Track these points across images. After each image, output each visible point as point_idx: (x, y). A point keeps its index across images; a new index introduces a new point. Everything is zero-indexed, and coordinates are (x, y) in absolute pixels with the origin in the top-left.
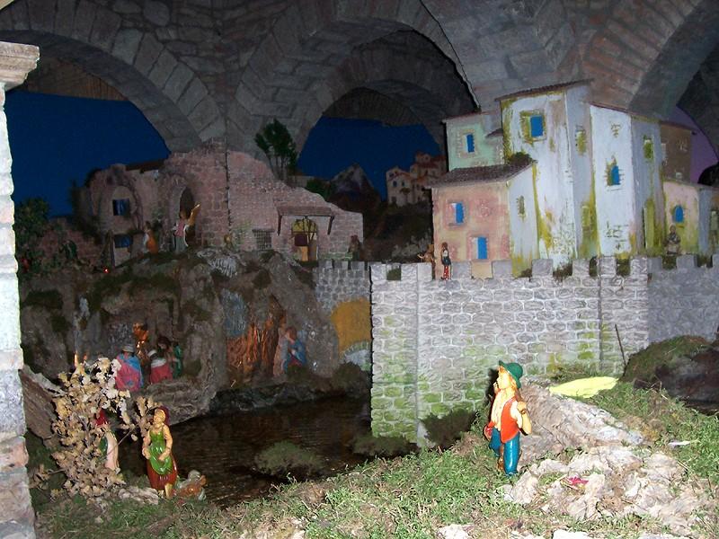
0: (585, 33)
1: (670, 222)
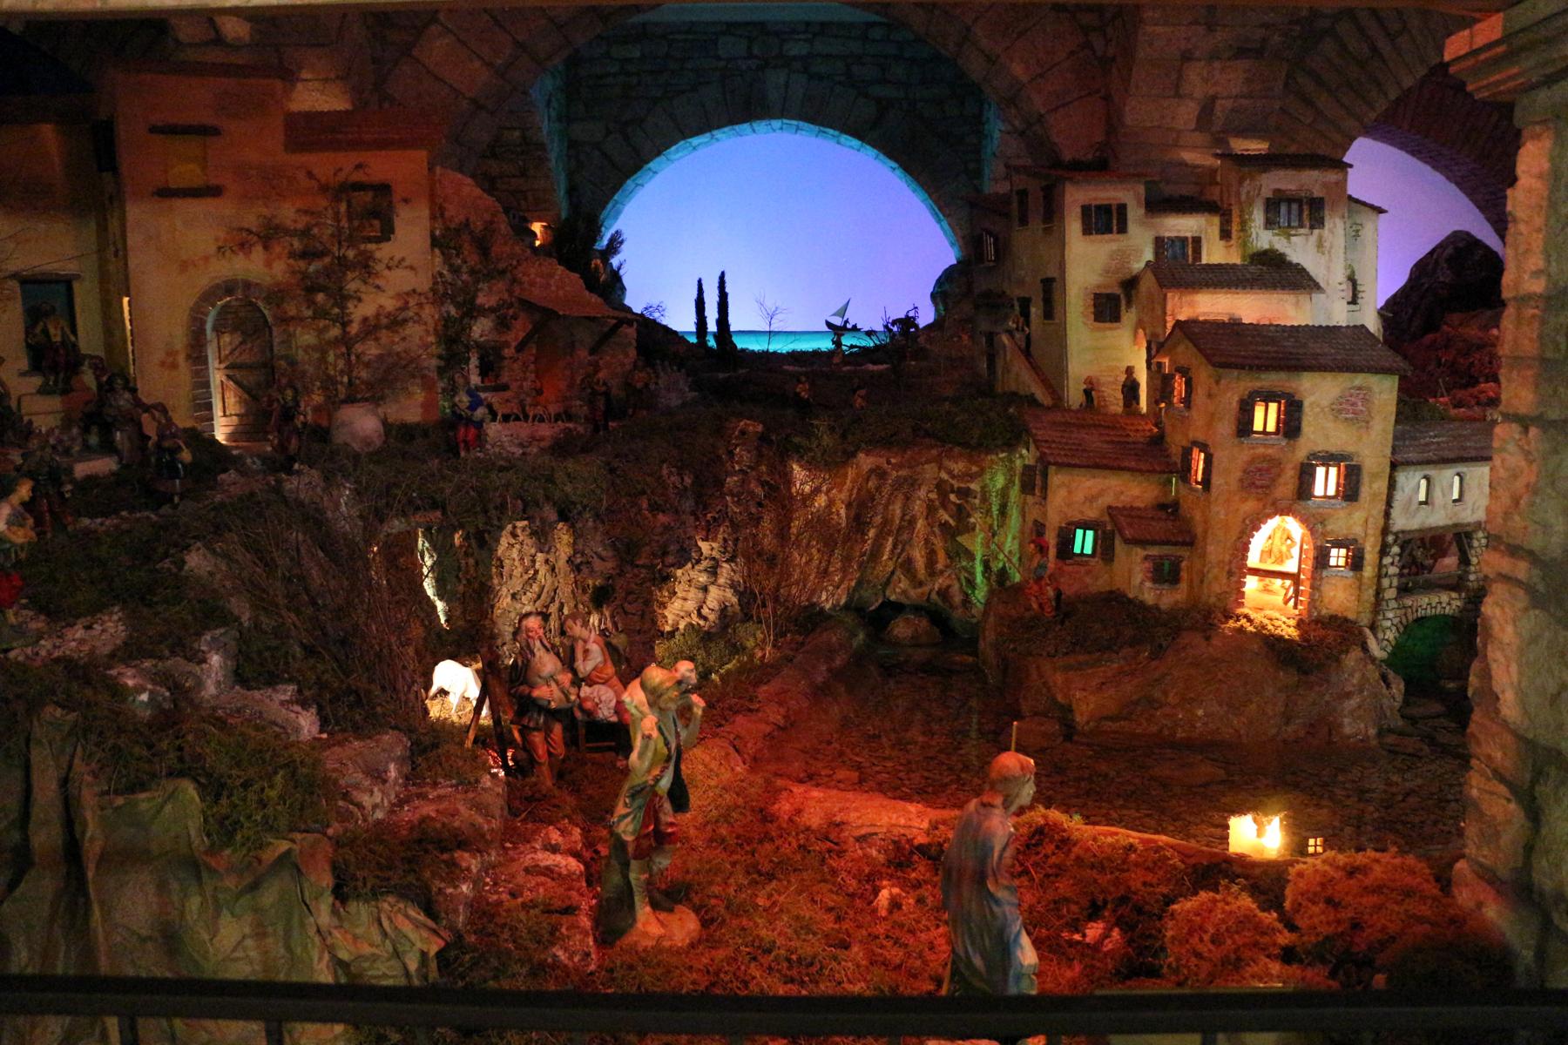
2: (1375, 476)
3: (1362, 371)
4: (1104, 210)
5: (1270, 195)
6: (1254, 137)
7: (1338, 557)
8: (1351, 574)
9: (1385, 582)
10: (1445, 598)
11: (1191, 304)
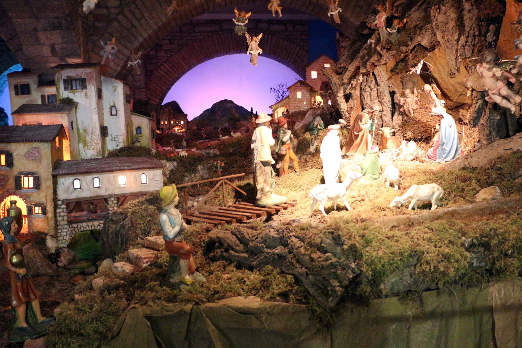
0: (92, 38)
1: (135, 132)
2: (47, 179)
3: (35, 141)
4: (22, 86)
5: (66, 78)
6: (74, 58)
7: (38, 210)
8: (43, 216)
9: (59, 219)
10: (96, 223)
11: (23, 119)
